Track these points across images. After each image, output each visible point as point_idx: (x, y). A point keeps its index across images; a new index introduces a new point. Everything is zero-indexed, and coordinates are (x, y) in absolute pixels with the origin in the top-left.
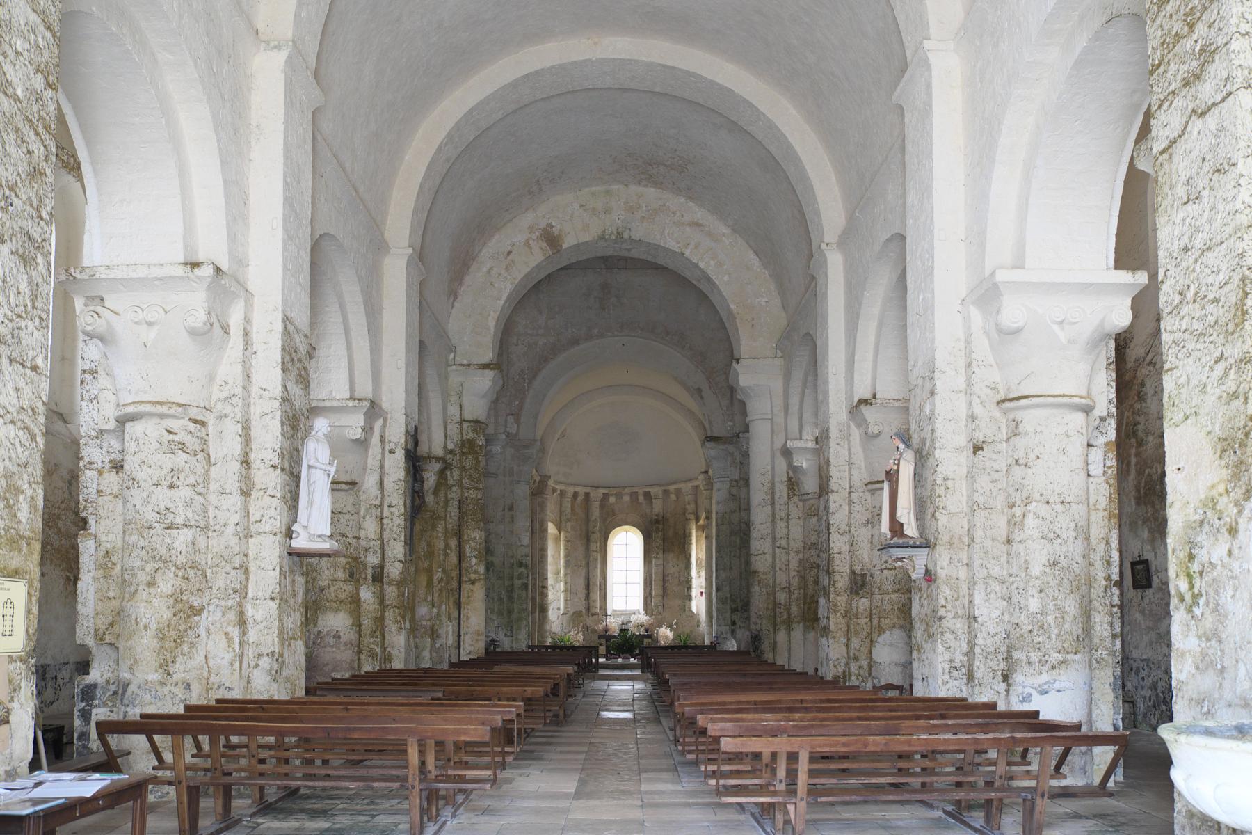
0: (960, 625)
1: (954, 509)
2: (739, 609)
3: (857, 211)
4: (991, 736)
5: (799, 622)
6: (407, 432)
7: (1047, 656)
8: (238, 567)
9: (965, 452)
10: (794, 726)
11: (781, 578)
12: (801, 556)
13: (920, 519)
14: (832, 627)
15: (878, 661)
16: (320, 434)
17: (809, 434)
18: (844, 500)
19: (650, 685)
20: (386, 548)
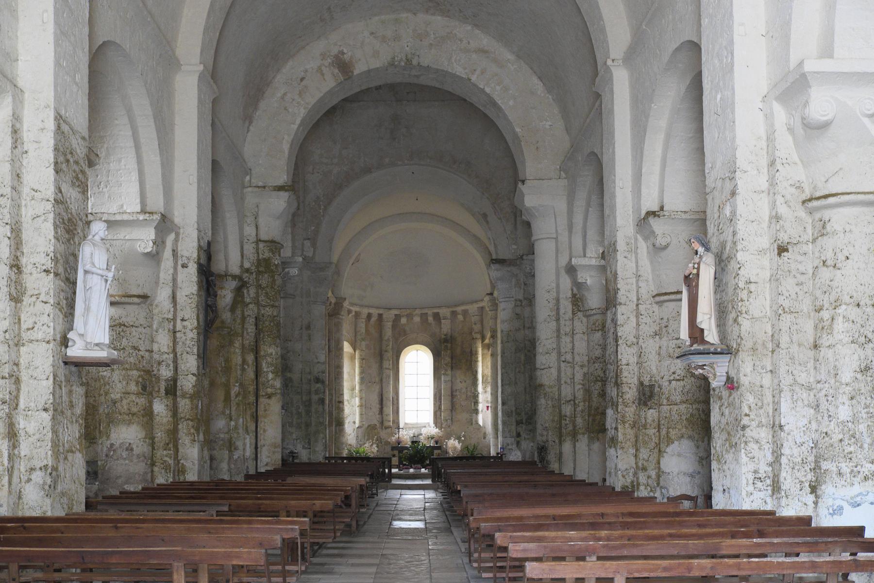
0: (764, 434)
1: (757, 313)
2: (524, 421)
3: (644, 23)
4: (466, 471)
5: (584, 434)
6: (200, 247)
7: (859, 467)
8: (7, 376)
9: (768, 254)
10: (604, 546)
11: (566, 392)
12: (585, 370)
13: (721, 324)
14: (621, 437)
15: (667, 471)
16: (97, 238)
17: (594, 251)
18: (632, 312)
19: (441, 495)
20: (180, 361)
